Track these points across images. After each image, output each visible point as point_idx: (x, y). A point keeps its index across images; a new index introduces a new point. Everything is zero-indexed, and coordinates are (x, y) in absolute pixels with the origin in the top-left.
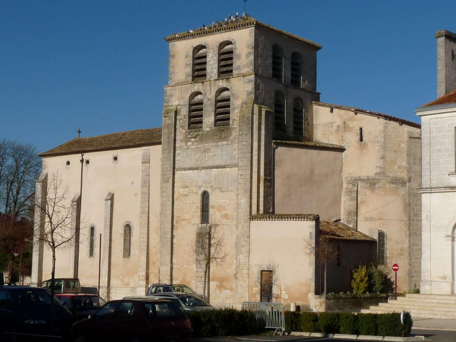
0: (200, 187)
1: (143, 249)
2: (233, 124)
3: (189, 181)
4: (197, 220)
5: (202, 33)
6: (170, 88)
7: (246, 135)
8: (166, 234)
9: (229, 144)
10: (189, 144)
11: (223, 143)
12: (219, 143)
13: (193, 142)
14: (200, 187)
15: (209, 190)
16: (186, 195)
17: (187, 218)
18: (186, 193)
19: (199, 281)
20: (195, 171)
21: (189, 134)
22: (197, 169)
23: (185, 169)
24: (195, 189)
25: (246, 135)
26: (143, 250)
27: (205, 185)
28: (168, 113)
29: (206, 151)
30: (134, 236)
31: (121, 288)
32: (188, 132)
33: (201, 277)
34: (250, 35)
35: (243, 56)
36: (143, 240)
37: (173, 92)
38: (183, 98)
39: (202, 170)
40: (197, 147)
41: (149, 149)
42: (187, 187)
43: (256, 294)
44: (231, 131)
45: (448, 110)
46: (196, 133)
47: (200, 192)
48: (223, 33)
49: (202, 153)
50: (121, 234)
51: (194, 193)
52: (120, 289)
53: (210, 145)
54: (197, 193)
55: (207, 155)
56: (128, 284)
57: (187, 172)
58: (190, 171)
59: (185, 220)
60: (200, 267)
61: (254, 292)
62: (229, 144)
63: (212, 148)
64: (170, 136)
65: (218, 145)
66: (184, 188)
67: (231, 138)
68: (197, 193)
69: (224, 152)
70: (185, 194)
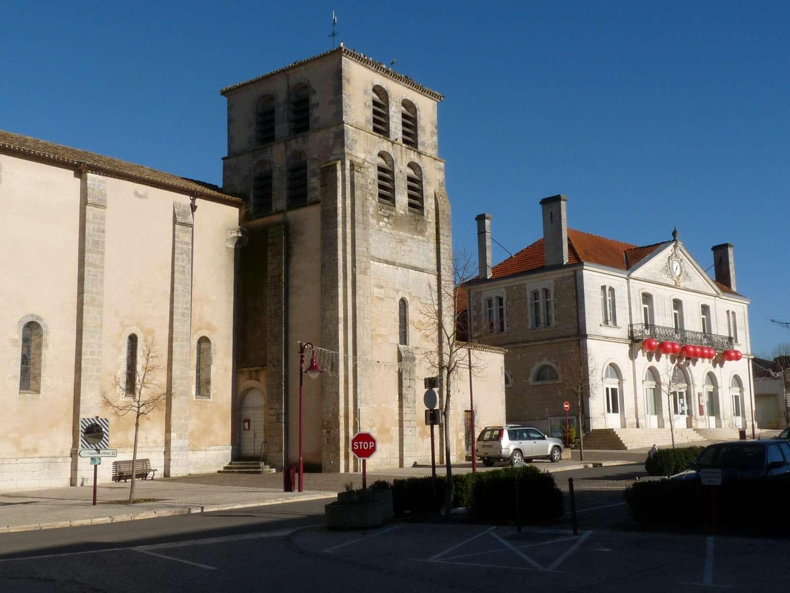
0: (398, 291)
1: (91, 376)
2: (427, 217)
3: (384, 278)
4: (396, 339)
5: (396, 77)
6: (352, 127)
7: (447, 236)
8: (365, 356)
9: (424, 241)
10: (381, 224)
11: (419, 237)
12: (415, 237)
13: (386, 223)
14: (398, 291)
15: (408, 299)
16: (381, 299)
17: (383, 333)
18: (381, 296)
19: (408, 427)
20: (391, 266)
21: (381, 210)
22: (393, 264)
23: (379, 260)
24: (391, 292)
25: (447, 236)
26: (93, 378)
27: (403, 289)
28: (361, 167)
29: (401, 241)
30: (50, 347)
31: (17, 459)
32: (380, 207)
33: (410, 421)
34: (433, 109)
35: (428, 132)
36: (94, 357)
37: (356, 137)
38: (370, 153)
39: (399, 268)
40: (392, 232)
41: (104, 182)
42: (381, 287)
43: (461, 440)
44: (426, 224)
45: (619, 275)
46: (389, 212)
47: (398, 300)
48: (417, 93)
49: (398, 242)
50: (15, 342)
51: (391, 298)
52: (14, 461)
53: (406, 236)
54: (394, 298)
55: (403, 248)
56: (35, 450)
57: (381, 264)
58: (385, 265)
59: (381, 336)
60: (409, 406)
61: (459, 438)
62: (424, 241)
63: (409, 240)
64: (365, 204)
65: (414, 238)
66: (379, 288)
67: (427, 234)
68: (394, 298)
69: (420, 250)
70: (380, 298)
